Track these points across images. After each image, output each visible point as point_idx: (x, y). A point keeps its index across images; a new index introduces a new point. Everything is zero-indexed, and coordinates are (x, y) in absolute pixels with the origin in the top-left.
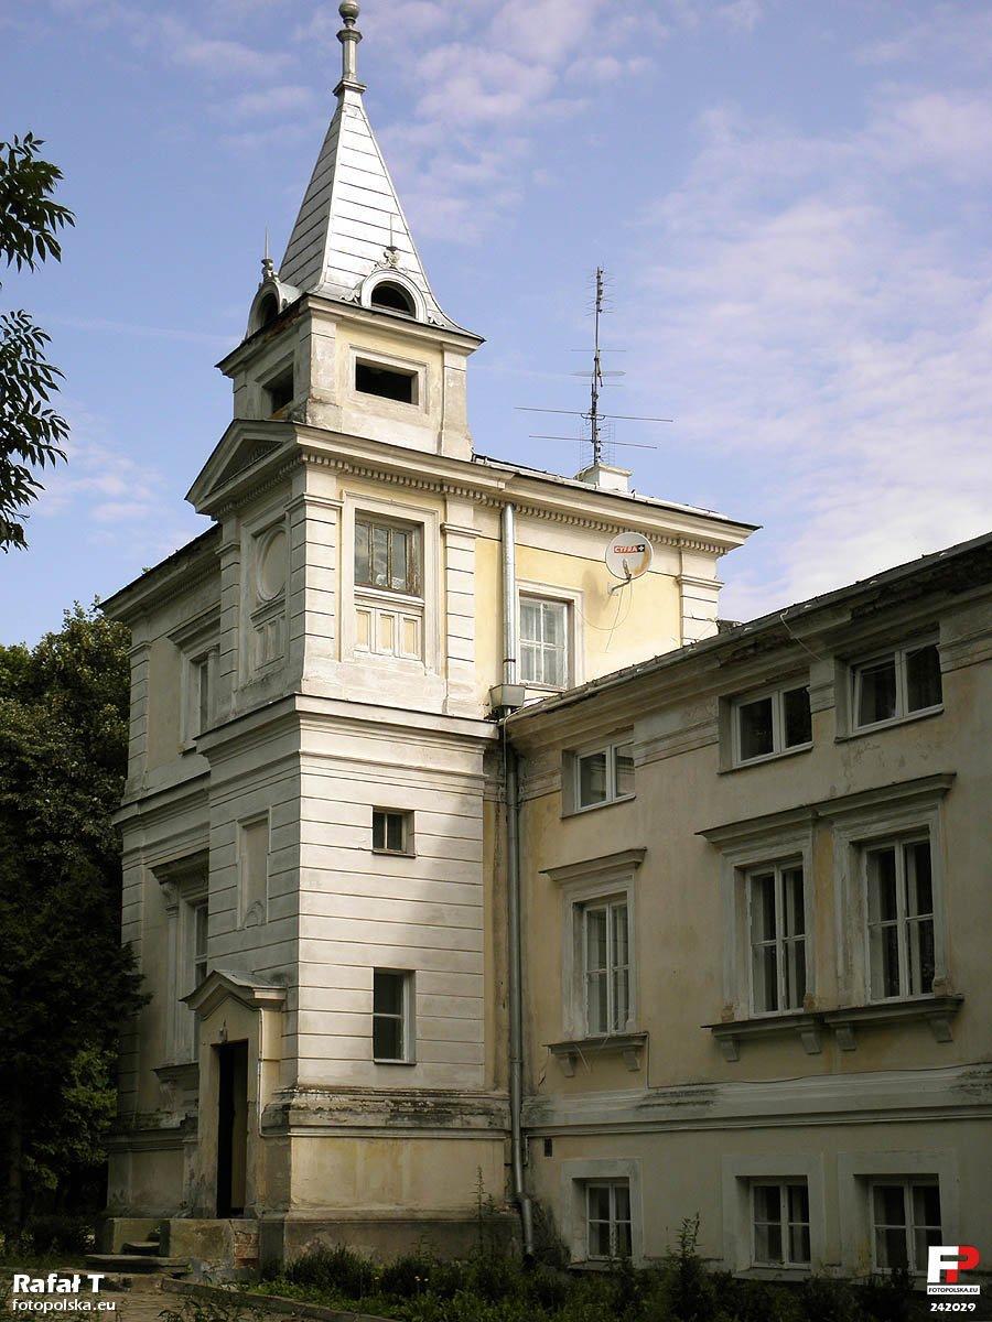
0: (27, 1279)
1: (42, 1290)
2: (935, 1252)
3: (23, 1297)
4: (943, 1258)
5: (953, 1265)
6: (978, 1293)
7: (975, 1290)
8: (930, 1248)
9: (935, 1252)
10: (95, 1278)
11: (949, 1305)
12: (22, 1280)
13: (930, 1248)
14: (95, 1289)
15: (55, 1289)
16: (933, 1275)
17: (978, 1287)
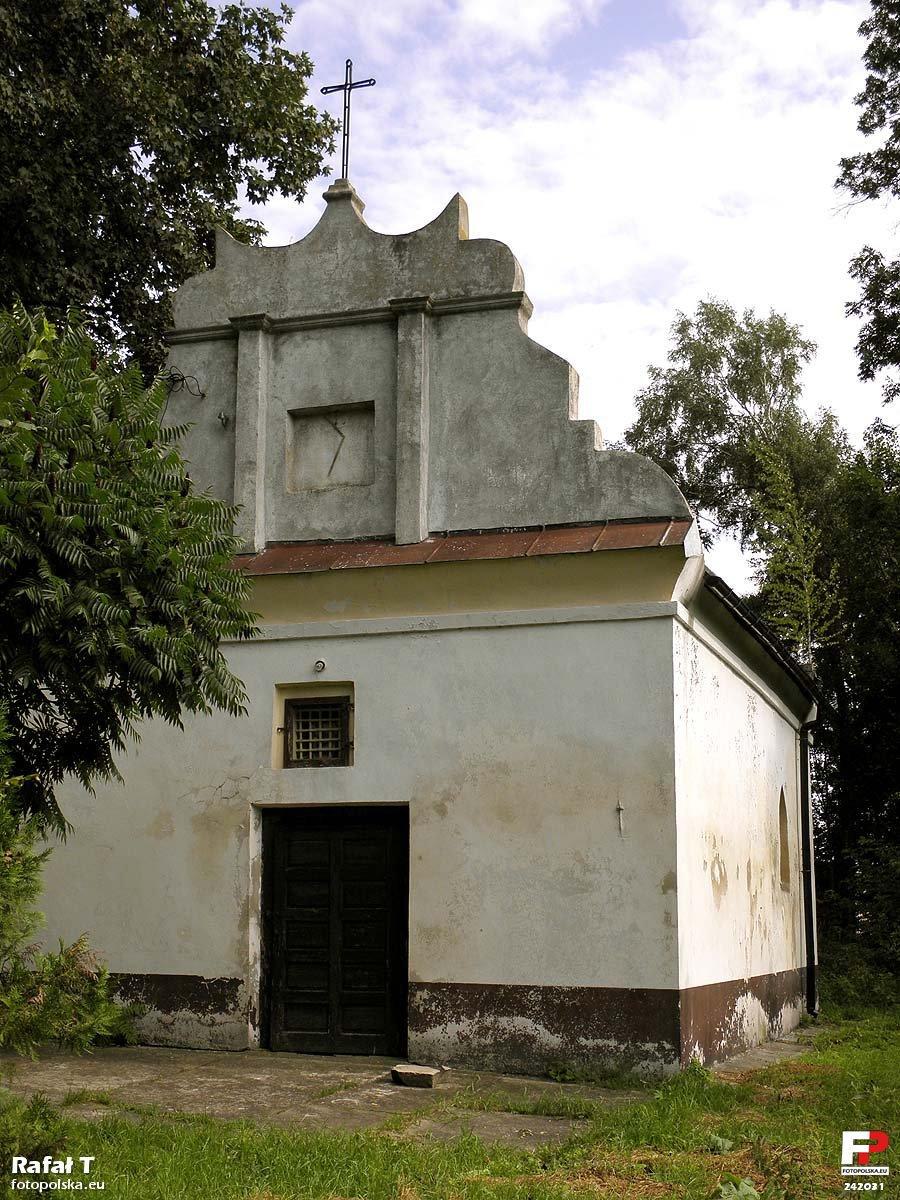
0: (24, 1161)
1: (38, 1171)
2: (848, 1137)
3: (852, 1180)
4: (856, 1142)
5: (865, 1149)
6: (887, 1174)
7: (885, 1170)
8: (844, 1133)
9: (848, 1137)
10: (87, 1160)
11: (861, 1185)
12: (20, 1162)
13: (844, 1133)
14: (86, 1170)
15: (50, 1171)
16: (847, 1158)
17: (888, 1168)
